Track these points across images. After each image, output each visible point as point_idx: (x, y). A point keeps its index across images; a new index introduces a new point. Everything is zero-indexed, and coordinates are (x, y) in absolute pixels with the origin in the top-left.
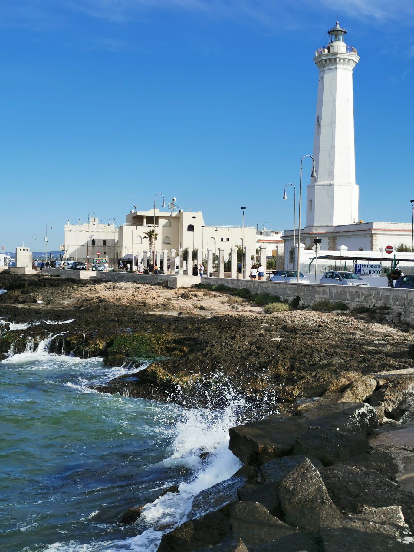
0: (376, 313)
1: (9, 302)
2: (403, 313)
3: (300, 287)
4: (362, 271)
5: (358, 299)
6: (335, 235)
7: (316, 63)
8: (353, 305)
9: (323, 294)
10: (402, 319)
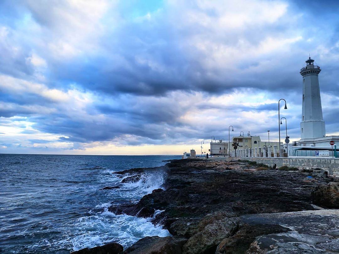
0: (313, 172)
1: (192, 165)
2: (329, 172)
3: (276, 159)
4: (319, 154)
5: (303, 165)
6: (314, 142)
7: (301, 74)
8: (69, 148)
9: (286, 163)
10: (328, 175)
